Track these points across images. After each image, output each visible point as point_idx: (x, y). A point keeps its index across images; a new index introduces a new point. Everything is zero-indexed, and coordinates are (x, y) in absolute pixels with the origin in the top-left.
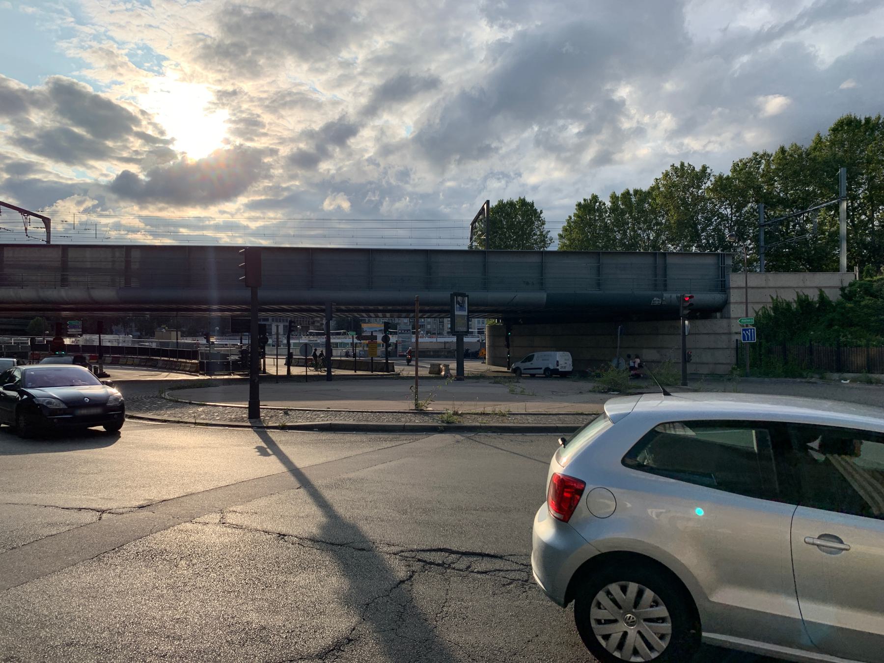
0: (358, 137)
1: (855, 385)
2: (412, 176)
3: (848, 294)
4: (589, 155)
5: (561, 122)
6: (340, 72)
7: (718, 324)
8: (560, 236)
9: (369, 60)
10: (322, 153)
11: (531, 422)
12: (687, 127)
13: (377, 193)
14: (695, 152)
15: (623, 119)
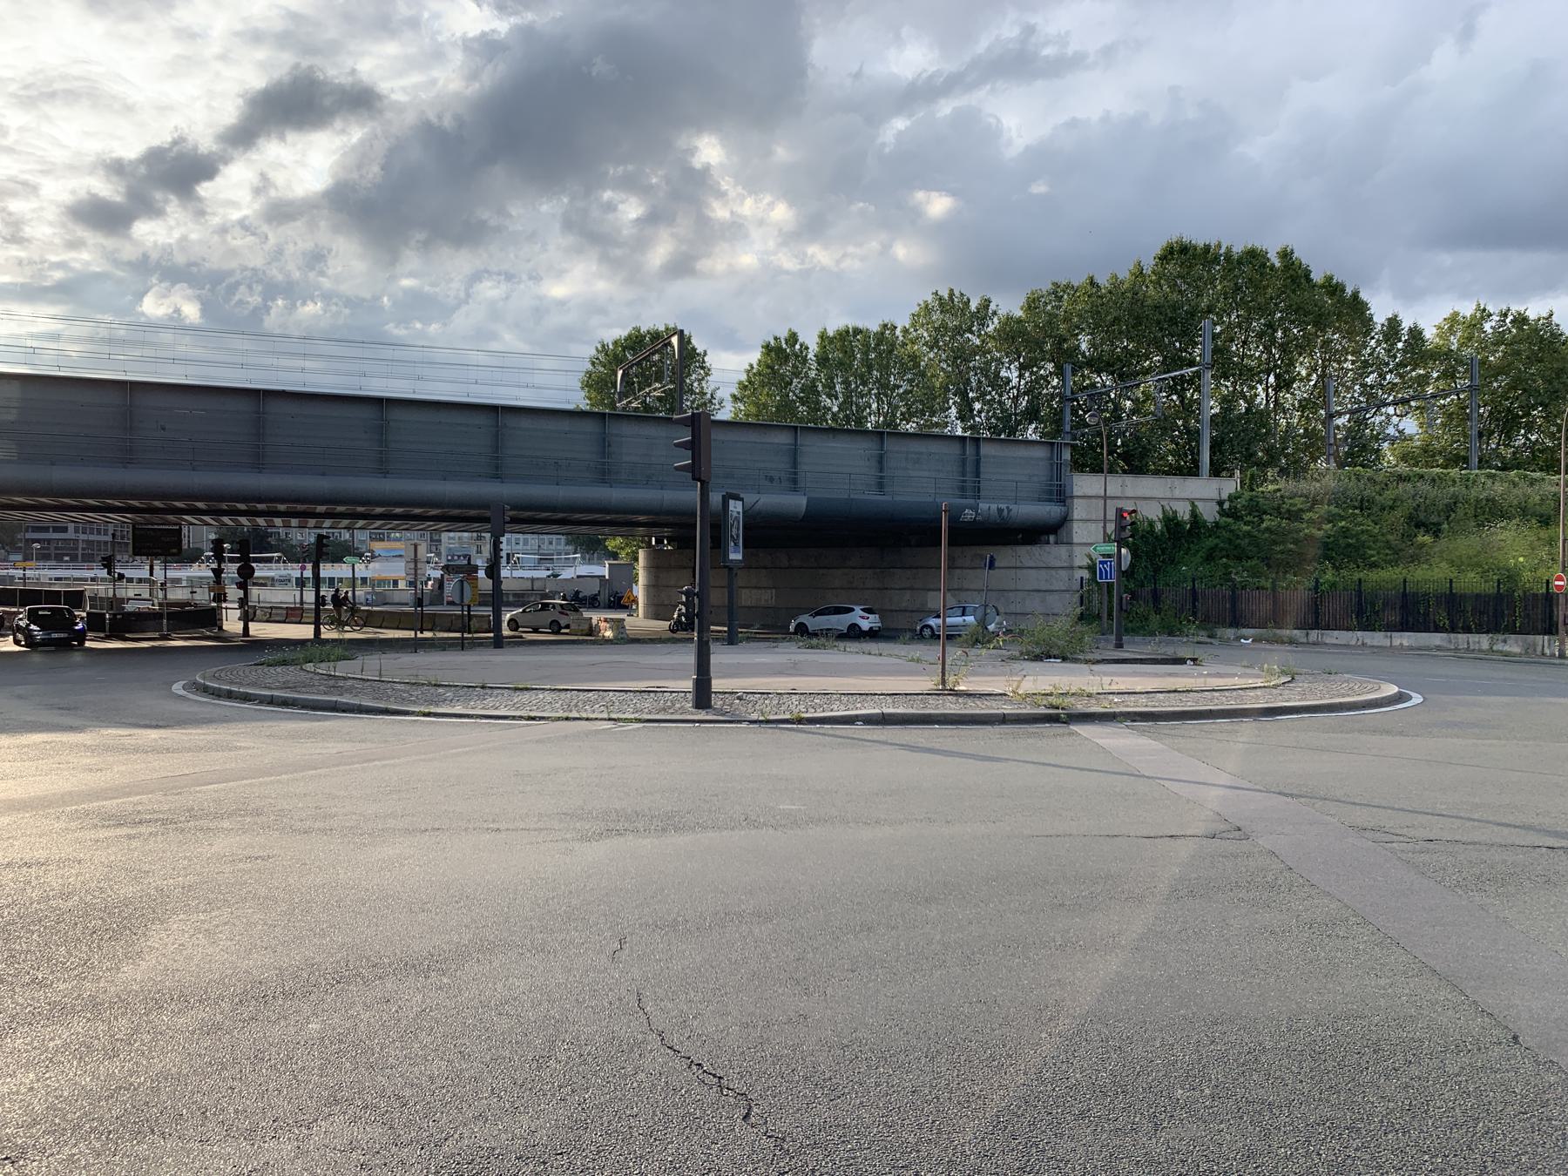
0: (219, 180)
1: (1258, 645)
2: (331, 262)
3: (1230, 510)
4: (660, 253)
5: (607, 195)
6: (177, 48)
7: (1052, 553)
8: (734, 396)
9: (237, 34)
10: (139, 205)
11: (1232, 705)
12: (812, 228)
13: (258, 288)
14: (823, 269)
15: (716, 204)
